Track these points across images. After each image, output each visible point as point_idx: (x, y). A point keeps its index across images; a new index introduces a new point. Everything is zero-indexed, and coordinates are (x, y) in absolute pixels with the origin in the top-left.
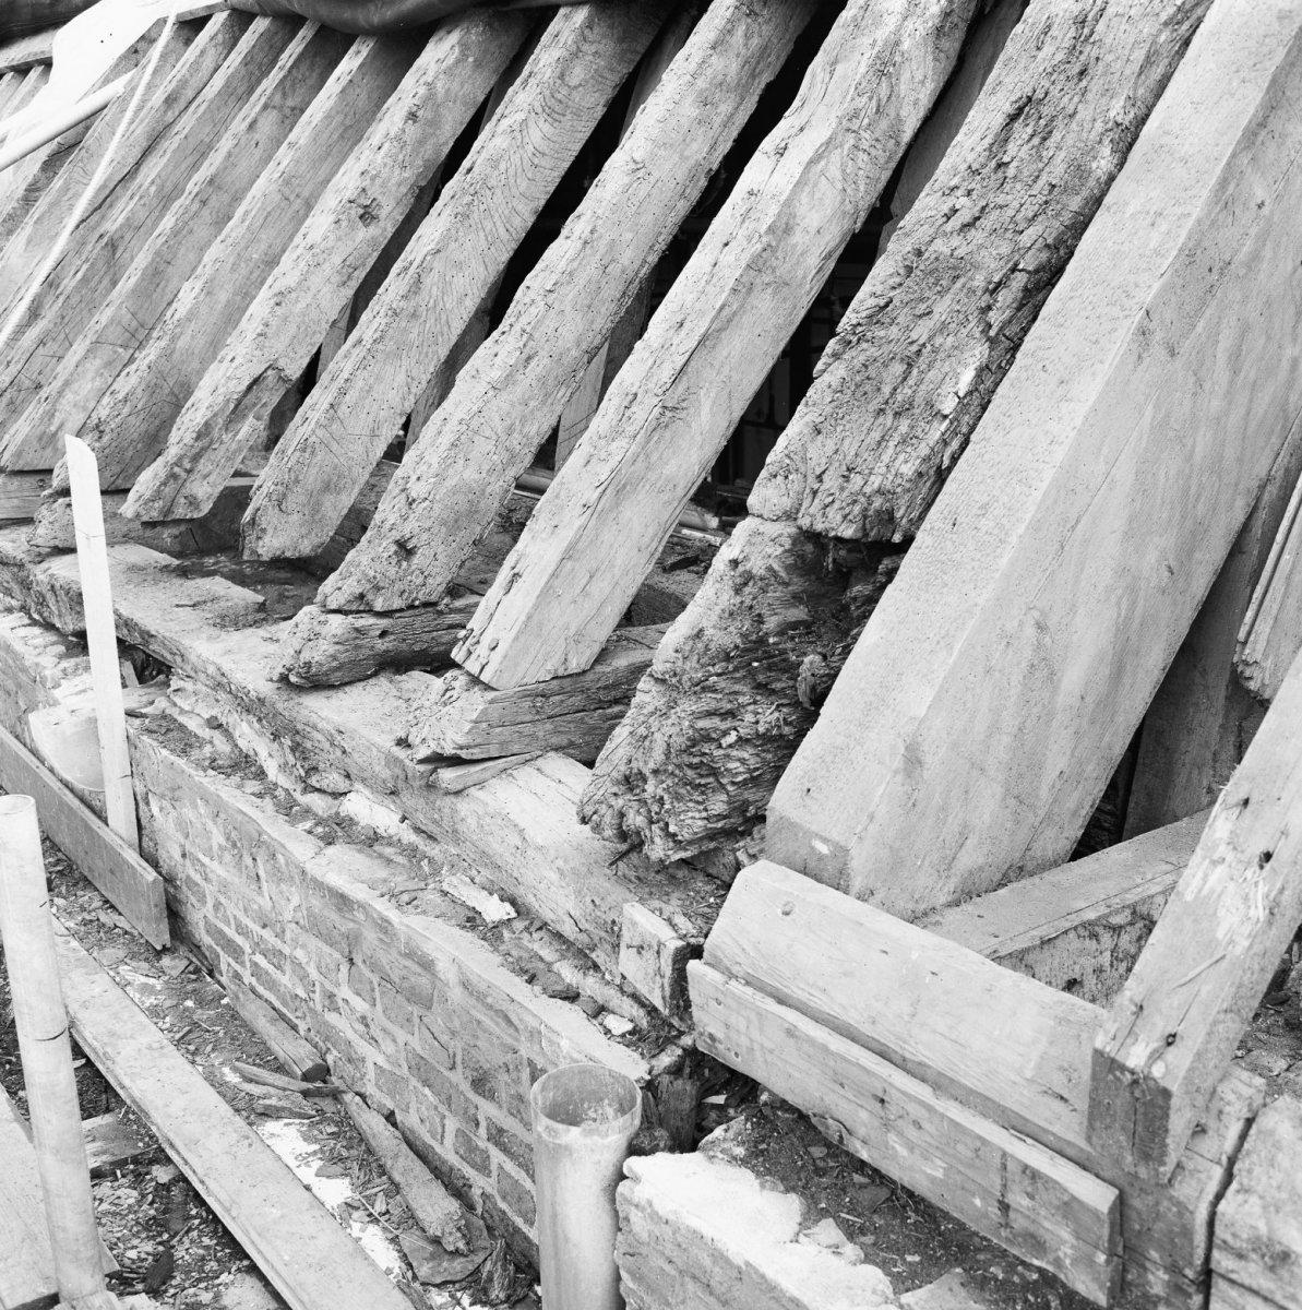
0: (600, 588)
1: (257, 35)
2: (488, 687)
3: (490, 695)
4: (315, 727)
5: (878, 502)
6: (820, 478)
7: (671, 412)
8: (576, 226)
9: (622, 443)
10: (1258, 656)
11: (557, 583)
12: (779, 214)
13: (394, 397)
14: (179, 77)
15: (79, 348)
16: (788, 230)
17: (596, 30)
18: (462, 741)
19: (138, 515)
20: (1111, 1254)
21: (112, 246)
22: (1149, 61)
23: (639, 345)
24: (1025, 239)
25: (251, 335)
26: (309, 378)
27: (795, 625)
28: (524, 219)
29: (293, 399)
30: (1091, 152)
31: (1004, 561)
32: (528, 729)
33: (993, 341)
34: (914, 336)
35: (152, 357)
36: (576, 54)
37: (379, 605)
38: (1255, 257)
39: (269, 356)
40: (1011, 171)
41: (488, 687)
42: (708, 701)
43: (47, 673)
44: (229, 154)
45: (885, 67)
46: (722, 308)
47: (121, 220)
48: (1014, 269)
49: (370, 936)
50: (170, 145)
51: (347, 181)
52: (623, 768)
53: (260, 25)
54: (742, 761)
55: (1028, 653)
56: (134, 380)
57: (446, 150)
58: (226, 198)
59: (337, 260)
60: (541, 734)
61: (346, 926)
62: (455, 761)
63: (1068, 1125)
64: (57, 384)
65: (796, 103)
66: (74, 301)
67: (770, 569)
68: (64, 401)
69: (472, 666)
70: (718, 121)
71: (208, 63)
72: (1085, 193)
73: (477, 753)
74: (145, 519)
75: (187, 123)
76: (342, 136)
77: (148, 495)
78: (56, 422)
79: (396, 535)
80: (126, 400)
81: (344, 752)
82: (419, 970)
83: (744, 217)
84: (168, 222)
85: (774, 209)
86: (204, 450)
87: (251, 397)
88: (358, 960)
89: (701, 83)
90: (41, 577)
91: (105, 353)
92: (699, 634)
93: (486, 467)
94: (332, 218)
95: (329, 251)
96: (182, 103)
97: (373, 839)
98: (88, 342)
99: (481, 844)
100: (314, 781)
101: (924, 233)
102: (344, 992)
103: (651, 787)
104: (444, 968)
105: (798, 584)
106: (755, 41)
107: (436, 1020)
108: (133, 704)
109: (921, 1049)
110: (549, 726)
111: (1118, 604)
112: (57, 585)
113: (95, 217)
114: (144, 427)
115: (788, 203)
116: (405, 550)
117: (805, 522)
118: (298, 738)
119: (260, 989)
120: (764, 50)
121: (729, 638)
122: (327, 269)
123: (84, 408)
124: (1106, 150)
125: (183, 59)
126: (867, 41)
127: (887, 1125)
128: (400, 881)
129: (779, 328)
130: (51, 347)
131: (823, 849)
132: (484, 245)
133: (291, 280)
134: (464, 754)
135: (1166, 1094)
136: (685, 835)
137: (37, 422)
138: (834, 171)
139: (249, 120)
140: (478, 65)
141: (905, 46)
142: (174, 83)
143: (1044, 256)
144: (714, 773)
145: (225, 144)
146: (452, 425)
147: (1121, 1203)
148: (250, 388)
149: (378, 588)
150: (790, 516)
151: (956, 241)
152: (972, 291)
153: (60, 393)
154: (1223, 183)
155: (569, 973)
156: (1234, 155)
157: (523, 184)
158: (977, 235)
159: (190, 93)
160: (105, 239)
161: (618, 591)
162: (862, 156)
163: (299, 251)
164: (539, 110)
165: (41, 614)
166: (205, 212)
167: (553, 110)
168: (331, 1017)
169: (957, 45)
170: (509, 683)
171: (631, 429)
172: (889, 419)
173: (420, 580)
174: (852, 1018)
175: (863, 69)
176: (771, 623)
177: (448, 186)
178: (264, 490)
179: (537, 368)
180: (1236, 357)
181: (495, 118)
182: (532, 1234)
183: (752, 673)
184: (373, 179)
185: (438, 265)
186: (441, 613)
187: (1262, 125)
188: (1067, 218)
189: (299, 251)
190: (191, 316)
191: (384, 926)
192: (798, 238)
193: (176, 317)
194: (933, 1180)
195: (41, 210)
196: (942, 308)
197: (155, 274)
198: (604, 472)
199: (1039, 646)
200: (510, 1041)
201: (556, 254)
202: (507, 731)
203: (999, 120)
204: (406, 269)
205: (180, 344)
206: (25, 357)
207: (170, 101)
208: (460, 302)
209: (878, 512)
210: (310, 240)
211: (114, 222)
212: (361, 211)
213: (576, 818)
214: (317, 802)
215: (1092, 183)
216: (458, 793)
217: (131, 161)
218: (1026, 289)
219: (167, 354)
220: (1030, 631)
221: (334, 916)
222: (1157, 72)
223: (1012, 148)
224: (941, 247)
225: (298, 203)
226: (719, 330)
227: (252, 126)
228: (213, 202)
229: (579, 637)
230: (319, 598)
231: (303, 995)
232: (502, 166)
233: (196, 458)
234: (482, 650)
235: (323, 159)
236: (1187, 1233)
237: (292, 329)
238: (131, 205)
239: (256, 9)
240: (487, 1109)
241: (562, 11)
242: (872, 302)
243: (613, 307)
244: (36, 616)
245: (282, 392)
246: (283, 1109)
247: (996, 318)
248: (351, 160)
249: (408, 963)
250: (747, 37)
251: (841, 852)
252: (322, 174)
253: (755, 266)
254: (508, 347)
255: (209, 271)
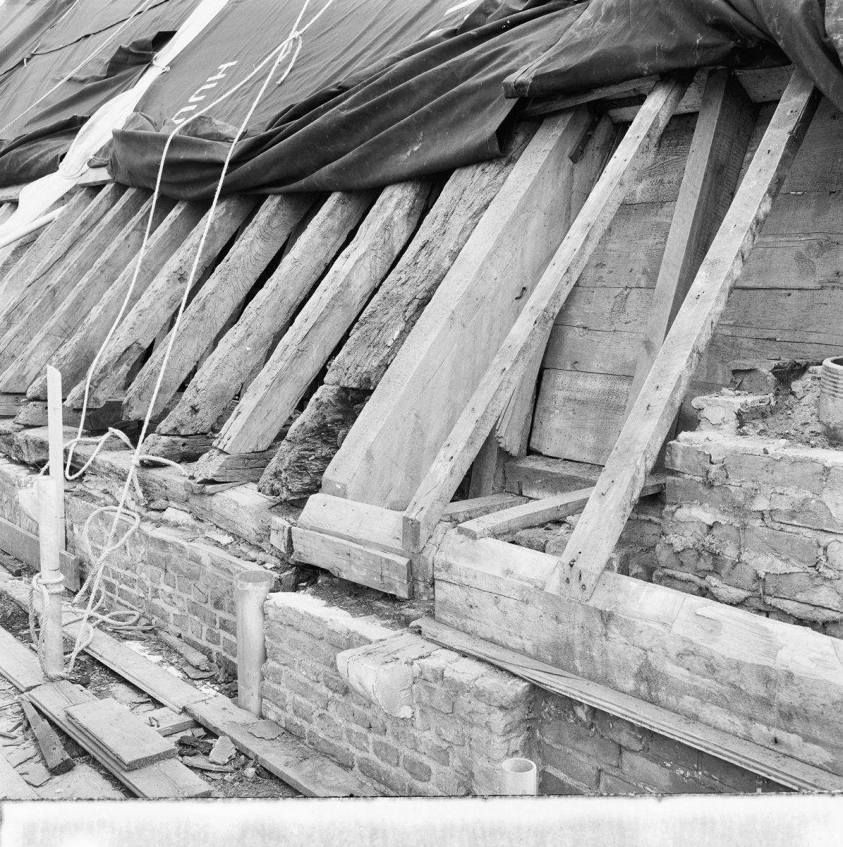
0: (272, 418)
1: (129, 196)
2: (227, 453)
3: (227, 456)
4: (154, 481)
5: (365, 375)
6: (348, 369)
7: (301, 352)
8: (270, 283)
9: (282, 363)
10: (503, 435)
11: (255, 414)
12: (344, 280)
13: (191, 354)
14: (88, 213)
15: (38, 337)
16: (348, 285)
17: (284, 205)
18: (215, 473)
19: (72, 405)
20: (408, 581)
21: (54, 291)
22: (463, 230)
23: (291, 328)
24: (419, 288)
25: (127, 329)
26: (148, 352)
27: (338, 420)
28: (251, 281)
29: (138, 365)
30: (442, 260)
31: (401, 392)
32: (242, 472)
33: (407, 322)
34: (382, 320)
35: (78, 339)
36: (275, 214)
37: (183, 432)
38: (495, 295)
39: (135, 338)
40: (419, 265)
41: (227, 453)
42: (305, 446)
43: (23, 479)
44: (116, 250)
45: (387, 227)
46: (322, 313)
47: (59, 279)
48: (415, 298)
49: (175, 555)
50: (85, 244)
51: (173, 263)
52: (274, 470)
53: (130, 192)
54: (316, 466)
55: (412, 424)
56: (69, 349)
57: (218, 252)
58: (112, 270)
59: (167, 297)
60: (247, 474)
61: (164, 555)
62: (212, 482)
63: (398, 545)
64: (28, 353)
65: (355, 239)
66: (34, 316)
67: (329, 400)
68: (30, 361)
69: (221, 447)
70: (330, 244)
71: (104, 206)
72: (440, 273)
73: (221, 479)
74: (75, 407)
75: (93, 235)
76: (170, 244)
77: (77, 396)
78: (26, 370)
79: (191, 404)
80: (65, 358)
81: (166, 489)
82: (194, 564)
83: (333, 281)
84: (84, 280)
85: (343, 278)
86: (103, 378)
87: (126, 356)
88: (169, 570)
89: (323, 229)
90: (20, 437)
91: (51, 339)
92: (303, 424)
93: (229, 378)
94: (166, 279)
95: (163, 293)
96: (89, 225)
97: (176, 526)
98: (43, 334)
99: (221, 513)
100: (152, 506)
101: (390, 286)
102: (163, 586)
103: (283, 475)
104: (206, 561)
105: (339, 407)
106: (346, 213)
107: (201, 584)
108: (67, 488)
109: (363, 535)
110: (250, 472)
111: (448, 412)
112: (29, 440)
113: (42, 278)
114: (72, 371)
115: (348, 275)
116: (194, 410)
117: (341, 384)
118: (146, 487)
119: (123, 601)
120: (349, 217)
121: (314, 424)
122: (163, 301)
123: (40, 365)
124: (447, 259)
125: (90, 205)
126: (380, 217)
127: (351, 563)
128: (188, 535)
129: (344, 322)
130: (21, 338)
131: (339, 487)
132: (232, 291)
133: (147, 305)
134: (216, 479)
135: (419, 523)
136: (294, 490)
137: (17, 370)
138: (367, 264)
139: (126, 235)
140: (233, 216)
141: (396, 219)
142: (86, 216)
143: (425, 294)
144: (306, 469)
145: (114, 245)
146: (216, 360)
147: (410, 564)
148: (125, 351)
149: (182, 425)
150: (337, 383)
151: (399, 289)
152: (401, 306)
153: (29, 357)
154: (480, 271)
155: (253, 554)
156: (484, 262)
157: (251, 267)
158: (406, 287)
159: (93, 221)
160: (51, 288)
161: (279, 420)
162: (378, 259)
163: (150, 293)
164: (258, 236)
165: (17, 457)
166: (103, 276)
167: (264, 237)
168: (155, 601)
169: (416, 220)
170: (235, 452)
171: (286, 358)
172: (371, 349)
173: (200, 423)
174: (343, 531)
175: (378, 227)
176: (328, 419)
177: (219, 266)
178: (133, 390)
179: (252, 339)
180: (490, 329)
181: (240, 239)
182: (235, 660)
183: (322, 437)
184: (185, 263)
185: (213, 299)
186: (208, 438)
187: (495, 252)
188: (433, 281)
189: (150, 293)
190: (96, 321)
191: (181, 550)
192: (352, 289)
193: (90, 321)
194: (364, 577)
195: (13, 274)
196: (392, 311)
197: (77, 304)
198: (274, 374)
199: (416, 423)
200: (228, 580)
201: (262, 294)
202: (233, 471)
203: (418, 248)
204: (199, 300)
205: (92, 333)
206: (8, 342)
207: (83, 224)
208: (222, 315)
209: (365, 379)
210: (155, 288)
211: (56, 277)
212: (179, 276)
213: (257, 490)
214: (153, 514)
215: (442, 270)
216: (213, 494)
217: (63, 252)
218: (418, 305)
219: (85, 338)
220: (413, 417)
221: (160, 553)
222: (466, 234)
223: (420, 257)
224: (394, 291)
225: (149, 273)
226: (321, 322)
227: (127, 238)
228: (106, 272)
229: (263, 437)
230: (157, 431)
231: (142, 595)
232: (242, 260)
233: (99, 381)
234: (225, 441)
235: (161, 254)
236: (426, 567)
237: (146, 326)
238: (65, 272)
239: (130, 184)
240: (221, 614)
241: (270, 197)
242: (371, 310)
243: (284, 316)
244: (14, 458)
245: (139, 354)
246: (133, 636)
247: (408, 314)
248: (175, 255)
249: (191, 562)
250: (342, 212)
251: (344, 486)
252: (161, 260)
253: (335, 298)
254: (240, 330)
255: (106, 302)
